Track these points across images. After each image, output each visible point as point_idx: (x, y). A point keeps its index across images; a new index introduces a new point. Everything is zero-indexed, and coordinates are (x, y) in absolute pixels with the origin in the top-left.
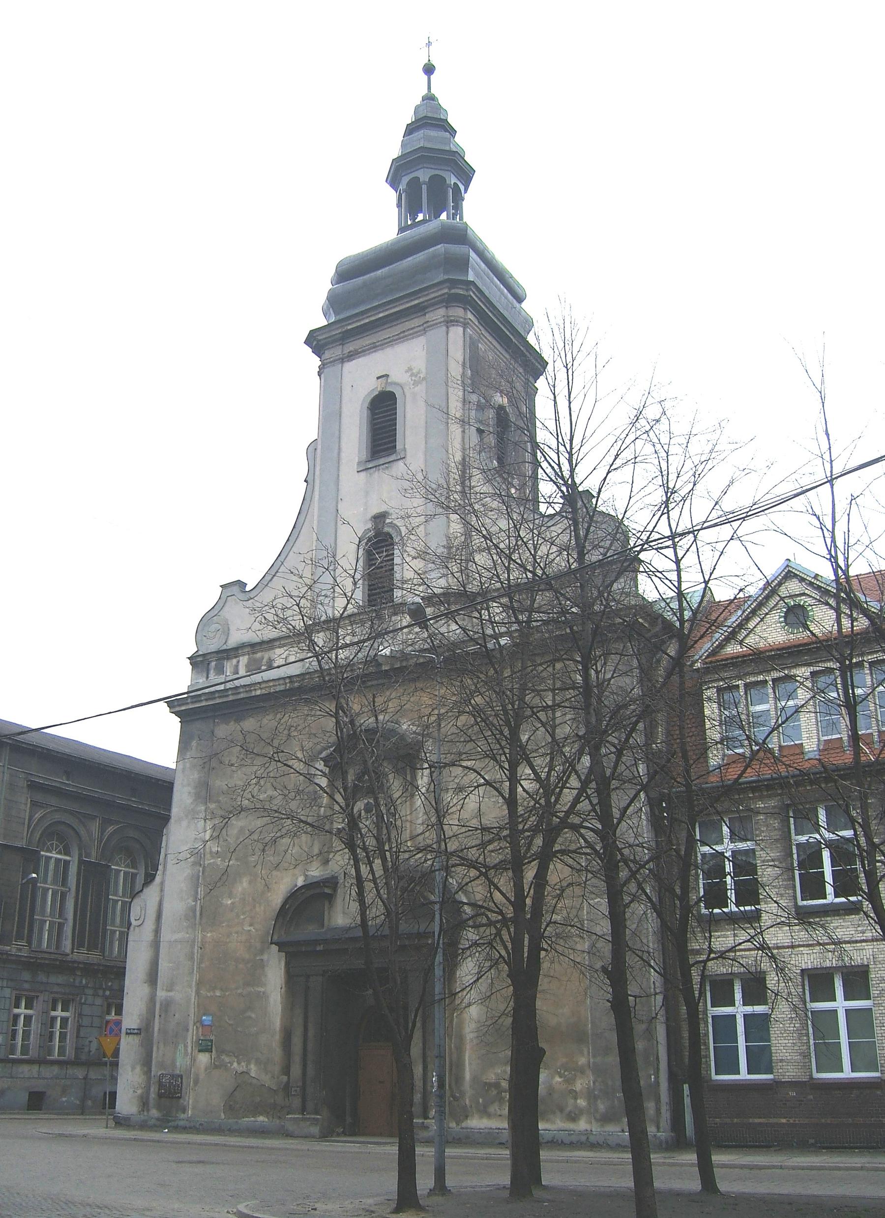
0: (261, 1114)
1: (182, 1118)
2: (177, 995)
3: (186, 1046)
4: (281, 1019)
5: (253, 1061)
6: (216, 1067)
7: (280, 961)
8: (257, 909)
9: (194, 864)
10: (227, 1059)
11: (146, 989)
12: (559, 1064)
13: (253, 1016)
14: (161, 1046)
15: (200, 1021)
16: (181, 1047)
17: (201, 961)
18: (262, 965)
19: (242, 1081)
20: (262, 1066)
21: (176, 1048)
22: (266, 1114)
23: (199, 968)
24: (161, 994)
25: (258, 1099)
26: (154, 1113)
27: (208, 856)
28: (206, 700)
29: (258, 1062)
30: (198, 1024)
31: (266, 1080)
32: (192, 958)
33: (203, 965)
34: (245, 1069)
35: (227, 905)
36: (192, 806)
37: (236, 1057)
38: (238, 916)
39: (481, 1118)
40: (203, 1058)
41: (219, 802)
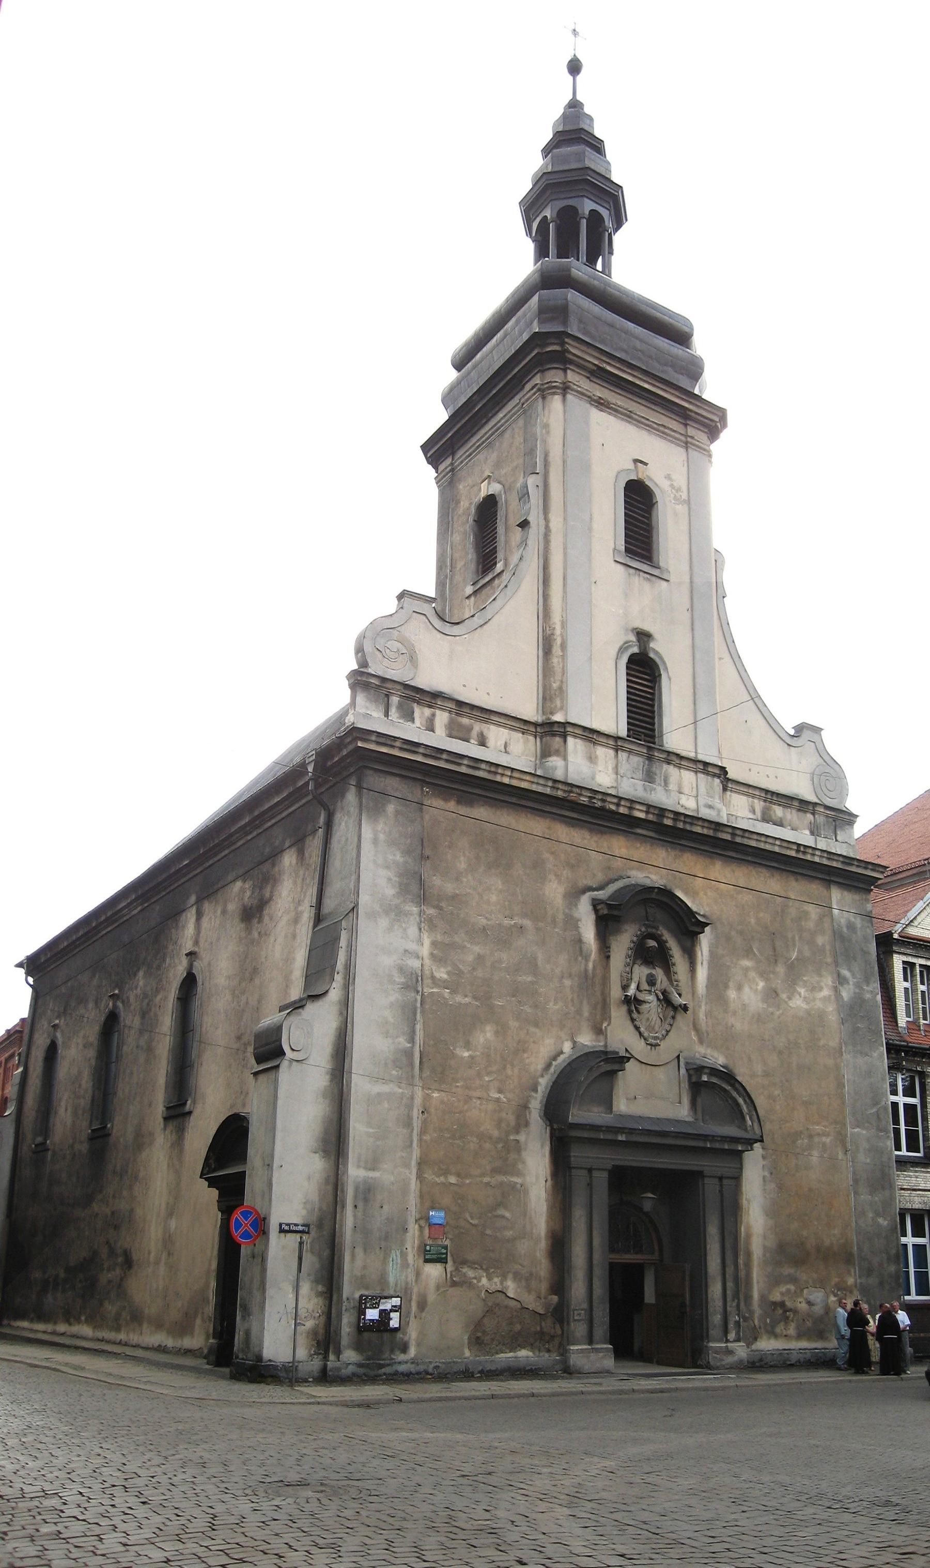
0: (522, 1347)
1: (404, 1361)
2: (385, 1176)
3: (404, 1255)
4: (547, 1222)
5: (510, 1276)
6: (454, 1284)
7: (542, 1146)
8: (509, 1072)
9: (406, 987)
10: (471, 1273)
11: (317, 1165)
12: (833, 1283)
13: (507, 1215)
14: (359, 1252)
15: (428, 1218)
16: (395, 1255)
17: (423, 1132)
18: (518, 1147)
19: (495, 1303)
20: (524, 1283)
21: (386, 1255)
22: (532, 1347)
23: (420, 1140)
24: (355, 1172)
25: (518, 1327)
26: (350, 1356)
27: (427, 981)
28: (425, 755)
29: (517, 1276)
30: (422, 1223)
31: (530, 1301)
32: (408, 1124)
33: (427, 1138)
34: (499, 1287)
35: (463, 1058)
36: (397, 901)
37: (486, 1270)
38: (479, 1075)
39: (769, 1339)
40: (434, 1271)
41: (441, 909)
